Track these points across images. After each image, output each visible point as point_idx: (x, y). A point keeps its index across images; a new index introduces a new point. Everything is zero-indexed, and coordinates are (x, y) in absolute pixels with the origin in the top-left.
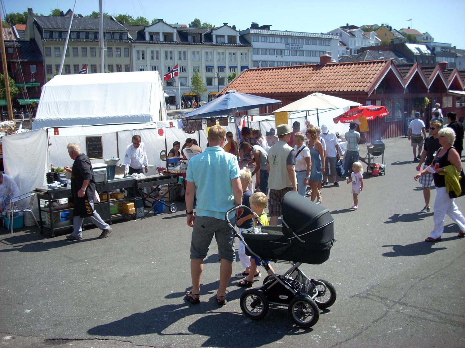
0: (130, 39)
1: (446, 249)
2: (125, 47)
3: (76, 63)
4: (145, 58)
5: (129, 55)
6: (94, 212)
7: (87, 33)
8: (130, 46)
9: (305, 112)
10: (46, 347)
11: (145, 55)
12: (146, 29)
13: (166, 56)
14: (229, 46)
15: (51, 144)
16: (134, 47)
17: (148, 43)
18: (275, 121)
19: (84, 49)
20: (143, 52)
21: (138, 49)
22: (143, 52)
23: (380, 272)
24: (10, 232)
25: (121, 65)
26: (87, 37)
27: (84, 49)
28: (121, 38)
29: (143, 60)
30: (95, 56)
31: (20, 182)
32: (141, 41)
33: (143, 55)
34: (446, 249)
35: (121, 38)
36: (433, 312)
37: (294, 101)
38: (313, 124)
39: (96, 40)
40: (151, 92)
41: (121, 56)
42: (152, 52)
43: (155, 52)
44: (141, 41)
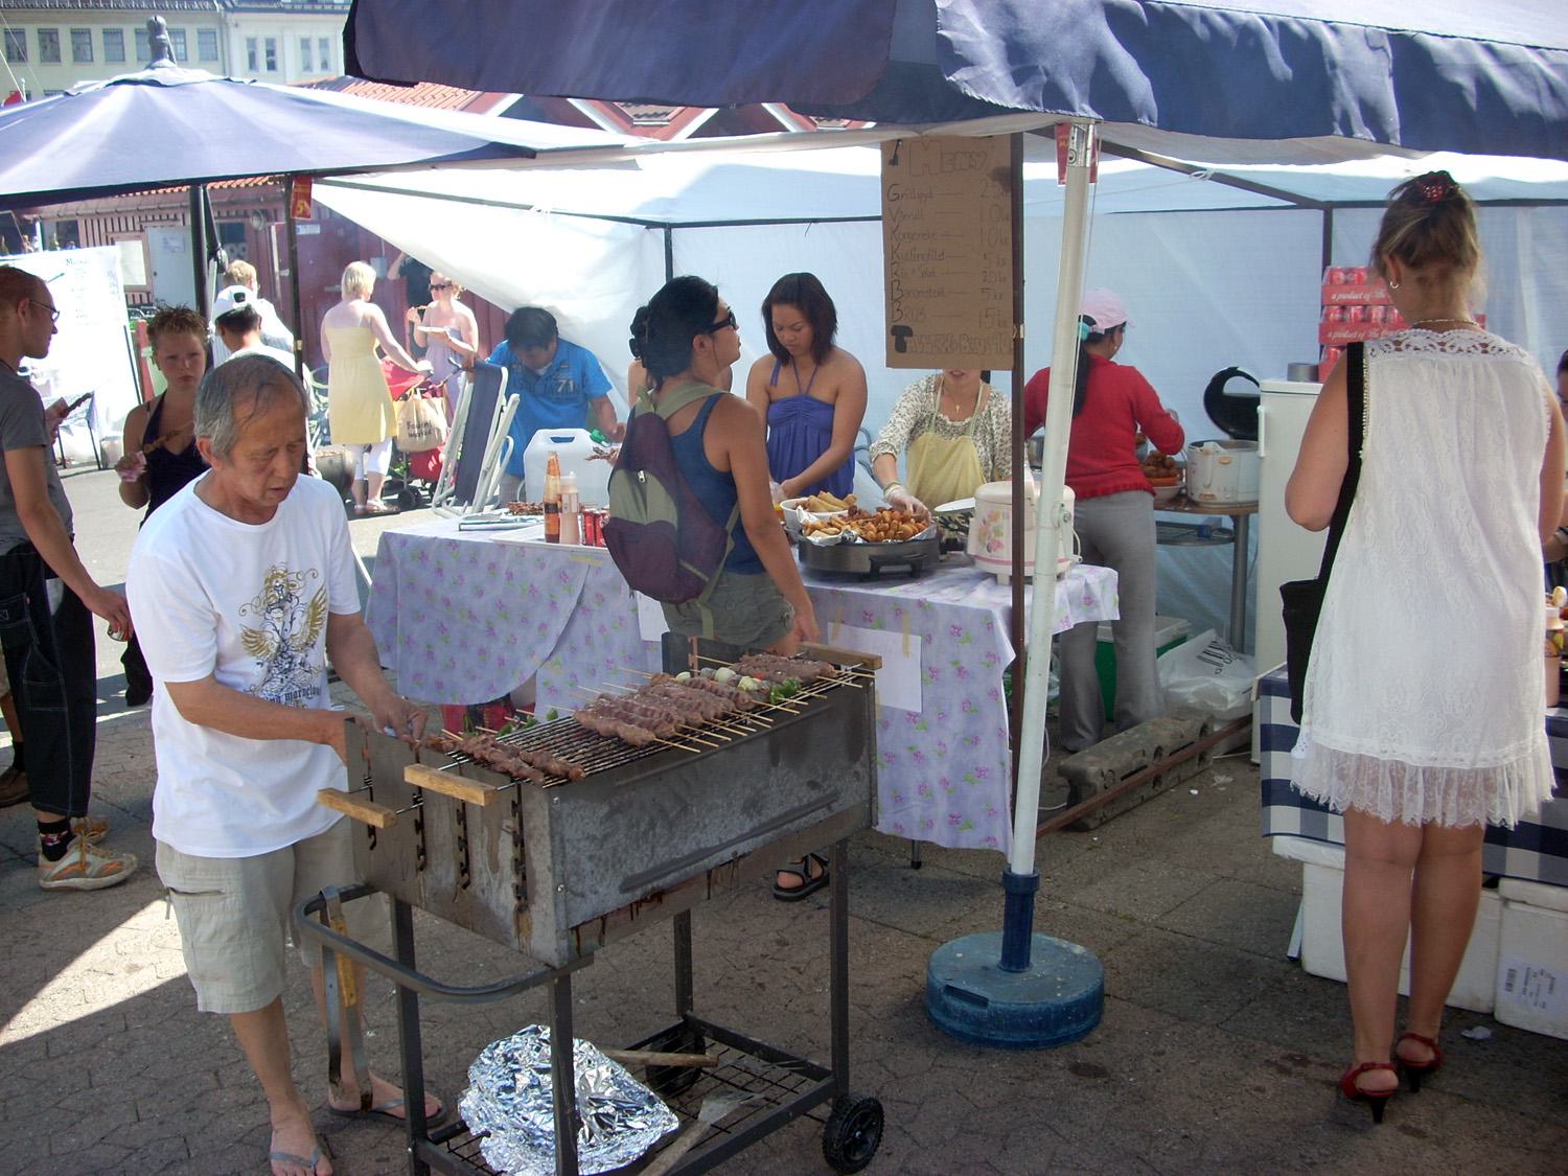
2: (202, 26)
4: (279, 65)
5: (220, 57)
8: (222, 22)
9: (661, 232)
11: (278, 52)
13: (271, 53)
16: (237, 25)
17: (288, 12)
18: (880, 223)
19: (49, 39)
20: (270, 42)
21: (251, 34)
22: (270, 42)
23: (1285, 1032)
24: (1329, 131)
27: (49, 39)
29: (272, 72)
30: (92, 60)
31: (583, 720)
32: (263, 6)
33: (271, 53)
36: (1453, 798)
37: (356, 226)
40: (480, 202)
41: (186, 59)
42: (305, 44)
43: (315, 45)
44: (263, 6)
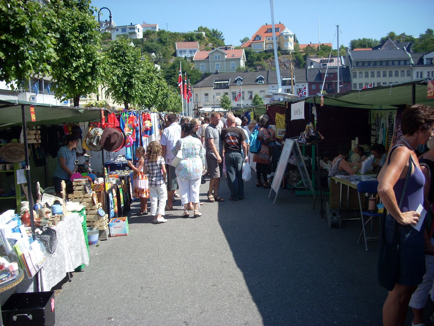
0: (412, 64)
1: (265, 33)
3: (397, 78)
6: (363, 162)
7: (399, 61)
8: (412, 69)
10: (244, 57)
11: (423, 74)
12: (424, 56)
13: (421, 74)
14: (431, 66)
15: (131, 24)
25: (359, 77)
26: (399, 64)
28: (405, 64)
33: (421, 74)
34: (265, 33)
35: (405, 64)
38: (205, 27)
39: (387, 66)
